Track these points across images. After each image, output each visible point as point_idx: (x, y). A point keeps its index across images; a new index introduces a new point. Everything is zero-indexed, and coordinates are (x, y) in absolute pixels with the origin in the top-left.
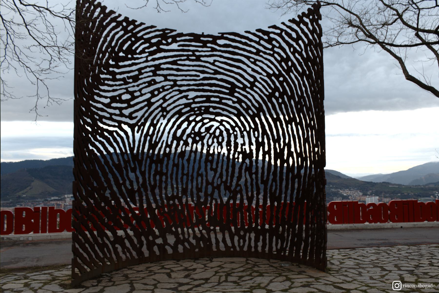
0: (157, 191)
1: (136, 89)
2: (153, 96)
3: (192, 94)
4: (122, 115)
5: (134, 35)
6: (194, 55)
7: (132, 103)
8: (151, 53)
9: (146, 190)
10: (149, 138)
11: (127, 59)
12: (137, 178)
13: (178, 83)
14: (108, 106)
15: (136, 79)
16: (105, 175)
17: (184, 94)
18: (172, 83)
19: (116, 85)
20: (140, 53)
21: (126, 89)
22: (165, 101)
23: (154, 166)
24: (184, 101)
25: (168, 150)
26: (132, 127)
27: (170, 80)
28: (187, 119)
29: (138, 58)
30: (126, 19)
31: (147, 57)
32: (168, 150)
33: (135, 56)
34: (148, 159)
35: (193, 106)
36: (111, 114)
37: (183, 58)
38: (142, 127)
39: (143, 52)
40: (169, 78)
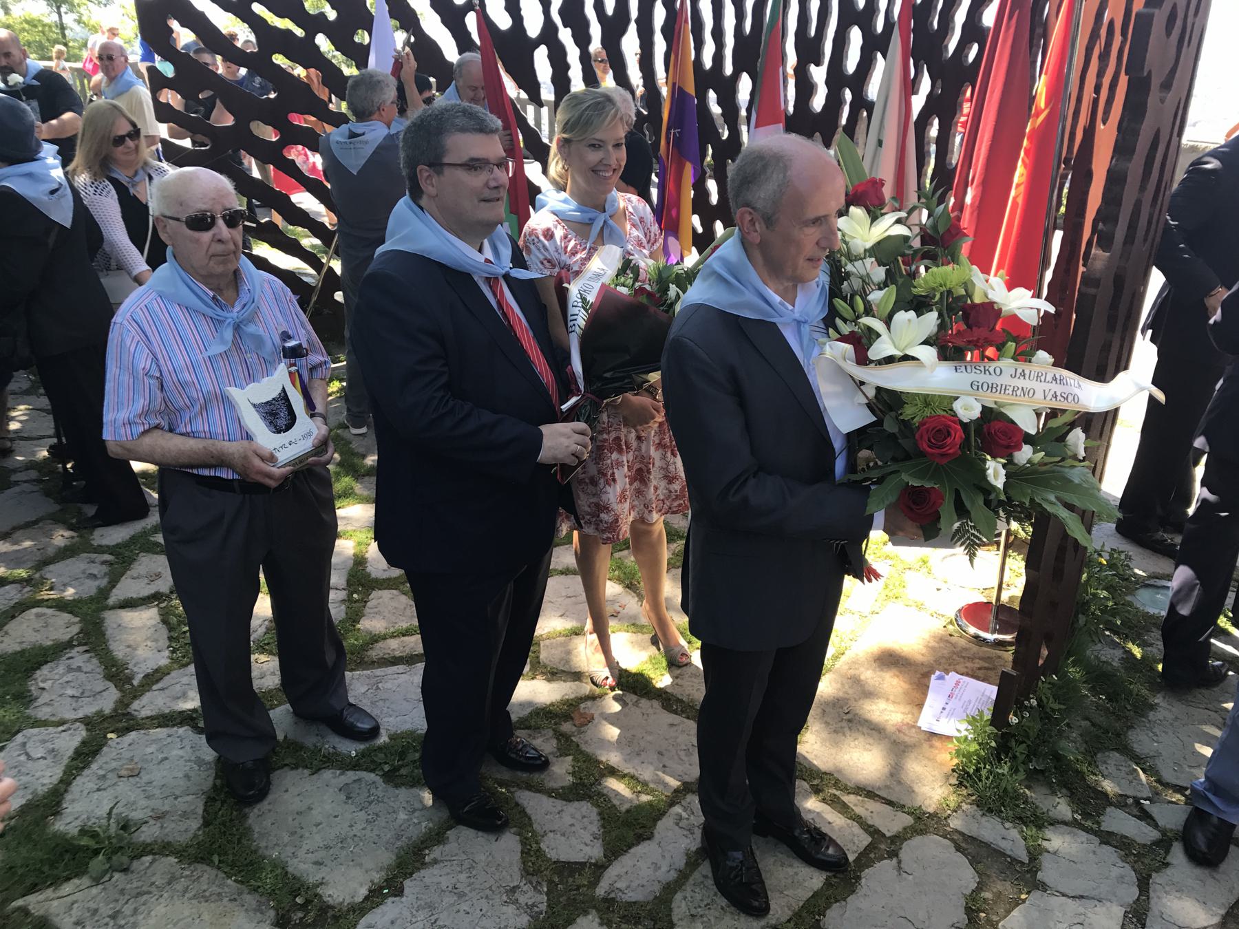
9: (582, 39)
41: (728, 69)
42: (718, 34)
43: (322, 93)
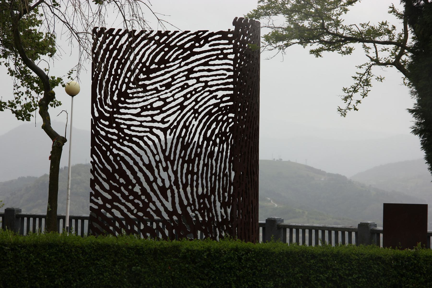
0: (189, 189)
1: (169, 95)
2: (186, 99)
3: (220, 94)
4: (153, 121)
5: (168, 45)
6: (222, 53)
7: (164, 109)
8: (184, 59)
9: (178, 188)
10: (181, 139)
11: (159, 69)
12: (169, 177)
13: (209, 84)
14: (138, 115)
15: (168, 86)
16: (134, 173)
17: (214, 94)
18: (203, 84)
19: (147, 96)
20: (174, 61)
21: (158, 96)
22: (197, 103)
23: (186, 165)
24: (214, 101)
25: (199, 150)
26: (164, 130)
27: (202, 82)
28: (216, 119)
29: (171, 66)
30: (159, 33)
31: (180, 63)
32: (199, 150)
33: (167, 65)
34: (181, 159)
35: (222, 105)
36: (141, 122)
37: (213, 58)
38: (175, 130)
39: (176, 59)
40: (201, 79)
41: (209, 194)
42: (207, 187)
43: (121, 198)
